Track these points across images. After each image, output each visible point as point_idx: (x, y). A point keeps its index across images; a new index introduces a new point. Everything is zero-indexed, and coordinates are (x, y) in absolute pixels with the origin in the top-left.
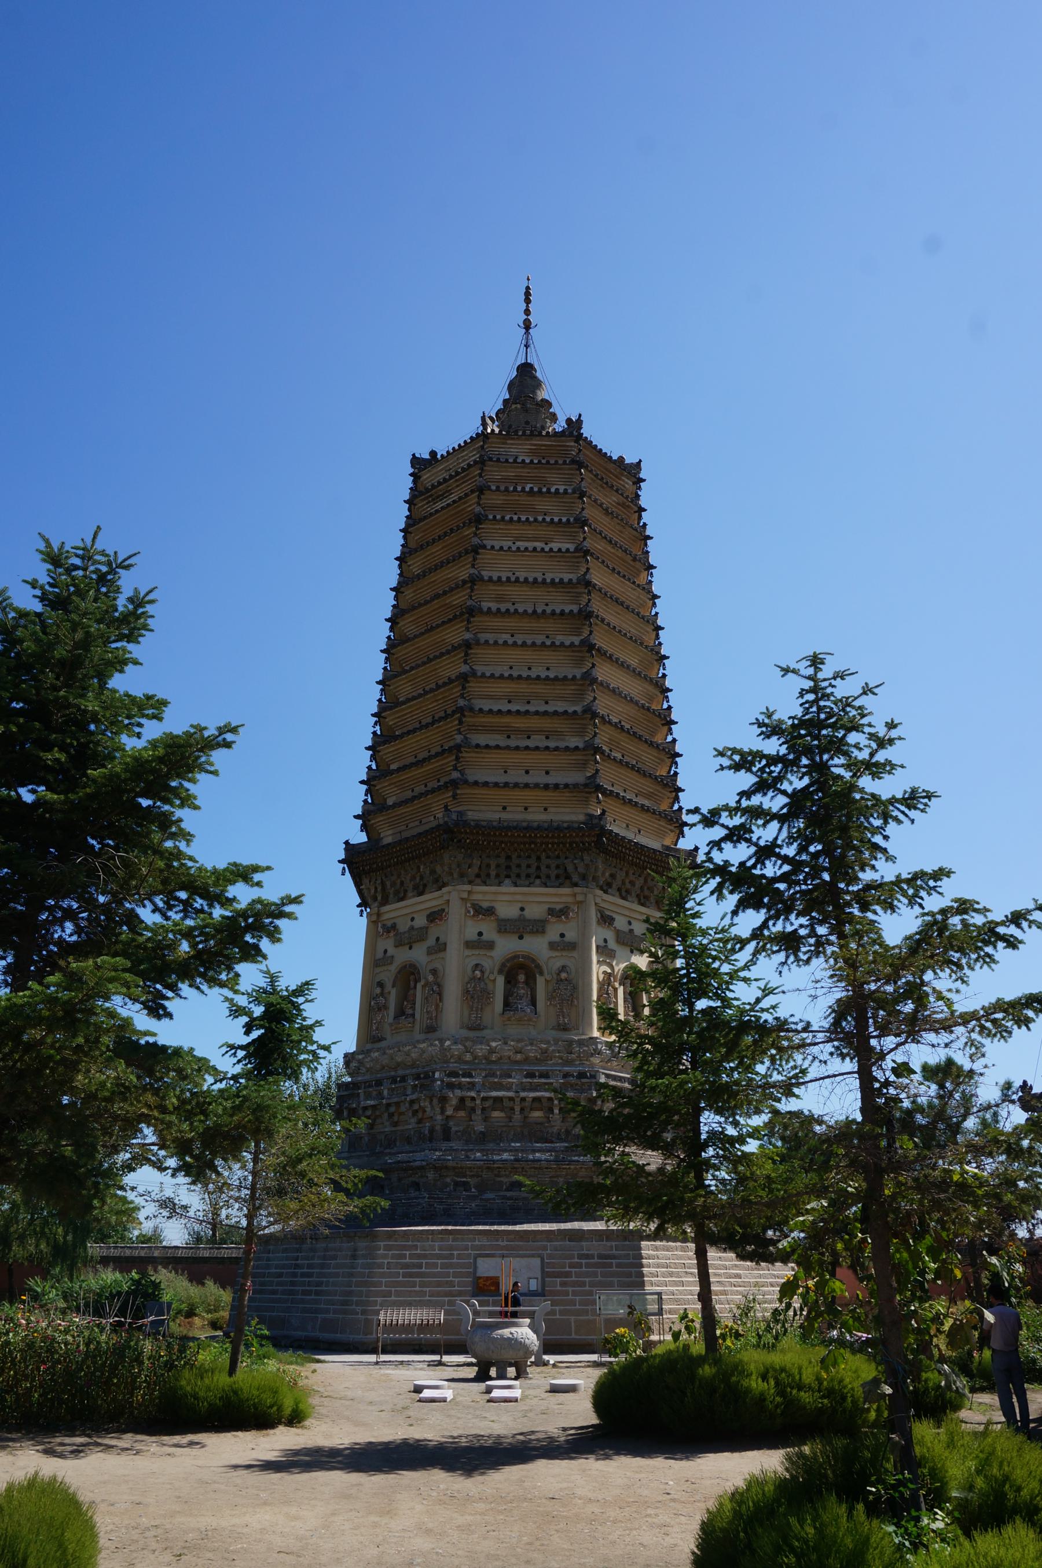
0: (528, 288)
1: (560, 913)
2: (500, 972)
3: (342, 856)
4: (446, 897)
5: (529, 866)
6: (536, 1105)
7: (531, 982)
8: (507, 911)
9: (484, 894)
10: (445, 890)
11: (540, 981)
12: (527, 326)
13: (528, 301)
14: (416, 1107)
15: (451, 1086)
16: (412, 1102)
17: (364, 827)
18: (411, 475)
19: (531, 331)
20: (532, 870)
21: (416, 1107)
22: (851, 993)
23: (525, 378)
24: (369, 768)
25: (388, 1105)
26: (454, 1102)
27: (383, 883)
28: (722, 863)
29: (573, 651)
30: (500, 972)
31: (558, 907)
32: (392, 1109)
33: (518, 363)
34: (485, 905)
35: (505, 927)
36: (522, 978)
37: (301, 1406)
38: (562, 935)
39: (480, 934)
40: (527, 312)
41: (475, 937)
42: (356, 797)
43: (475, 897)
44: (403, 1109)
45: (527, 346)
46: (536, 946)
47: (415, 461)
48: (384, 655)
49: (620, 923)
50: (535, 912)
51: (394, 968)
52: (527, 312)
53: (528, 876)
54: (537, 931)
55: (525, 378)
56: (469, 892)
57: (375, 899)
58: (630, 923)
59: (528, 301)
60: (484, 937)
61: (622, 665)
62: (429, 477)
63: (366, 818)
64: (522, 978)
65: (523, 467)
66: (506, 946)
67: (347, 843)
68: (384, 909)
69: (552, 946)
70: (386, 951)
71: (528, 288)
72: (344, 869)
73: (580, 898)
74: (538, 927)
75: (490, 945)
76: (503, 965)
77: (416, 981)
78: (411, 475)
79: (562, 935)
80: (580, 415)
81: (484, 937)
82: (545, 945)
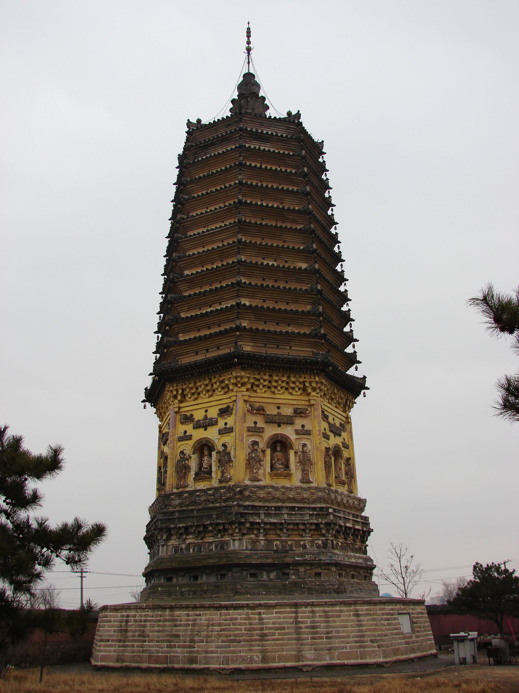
0: (249, 29)
2: (267, 447)
4: (234, 398)
9: (261, 397)
12: (249, 50)
13: (249, 36)
22: (469, 587)
23: (249, 87)
28: (334, 233)
33: (243, 73)
35: (270, 420)
38: (303, 426)
39: (255, 423)
40: (249, 43)
43: (252, 399)
45: (249, 63)
47: (189, 124)
51: (191, 443)
52: (249, 43)
55: (249, 87)
59: (249, 36)
60: (258, 425)
61: (331, 304)
66: (271, 431)
68: (182, 405)
71: (249, 29)
76: (268, 444)
79: (303, 426)
81: (258, 425)
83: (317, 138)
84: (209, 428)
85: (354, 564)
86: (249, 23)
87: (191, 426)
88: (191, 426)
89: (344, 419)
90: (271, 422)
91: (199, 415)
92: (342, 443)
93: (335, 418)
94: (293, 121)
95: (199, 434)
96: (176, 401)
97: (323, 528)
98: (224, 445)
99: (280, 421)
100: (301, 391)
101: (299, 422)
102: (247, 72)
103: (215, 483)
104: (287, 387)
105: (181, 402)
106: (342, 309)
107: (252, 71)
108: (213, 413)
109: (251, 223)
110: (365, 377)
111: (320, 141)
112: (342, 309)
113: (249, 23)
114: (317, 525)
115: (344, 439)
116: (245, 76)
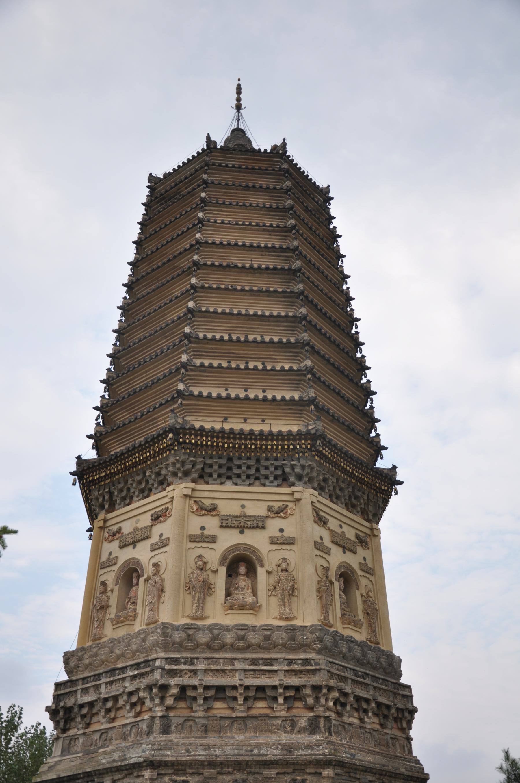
1: (279, 512)
3: (74, 468)
5: (249, 467)
6: (260, 695)
7: (251, 572)
8: (228, 508)
9: (208, 491)
10: (169, 489)
11: (261, 572)
12: (239, 107)
14: (134, 699)
15: (172, 673)
16: (131, 694)
17: (97, 446)
18: (148, 187)
19: (241, 111)
20: (252, 471)
21: (134, 699)
24: (103, 397)
25: (106, 700)
26: (175, 691)
27: (111, 494)
29: (285, 297)
30: (222, 563)
31: (277, 505)
32: (109, 704)
33: (232, 128)
34: (207, 503)
36: (242, 569)
37: (250, 643)
41: (199, 532)
42: (89, 421)
43: (197, 494)
44: (121, 702)
46: (257, 540)
48: (120, 311)
49: (333, 524)
50: (256, 510)
53: (248, 477)
54: (257, 527)
56: (193, 490)
57: (102, 507)
58: (341, 527)
62: (161, 189)
63: (98, 439)
64: (242, 569)
65: (240, 172)
66: (229, 539)
67: (79, 458)
69: (273, 541)
70: (110, 554)
72: (75, 480)
73: (297, 496)
74: (258, 524)
75: (213, 539)
77: (138, 577)
78: (148, 187)
80: (284, 140)
82: (267, 541)
83: (321, 183)
84: (139, 545)
85: (233, 758)
86: (239, 80)
87: (116, 544)
88: (116, 544)
89: (368, 531)
90: (227, 527)
91: (127, 528)
92: (360, 564)
93: (343, 524)
94: (280, 152)
95: (125, 555)
96: (104, 512)
97: (309, 696)
98: (156, 565)
99: (244, 524)
100: (279, 481)
101: (274, 526)
102: (236, 127)
103: (138, 626)
104: (257, 475)
105: (108, 512)
106: (362, 382)
107: (241, 126)
108: (146, 520)
109: (290, 343)
110: (394, 467)
111: (325, 186)
112: (362, 382)
113: (239, 80)
114: (297, 689)
115: (365, 559)
116: (233, 131)
